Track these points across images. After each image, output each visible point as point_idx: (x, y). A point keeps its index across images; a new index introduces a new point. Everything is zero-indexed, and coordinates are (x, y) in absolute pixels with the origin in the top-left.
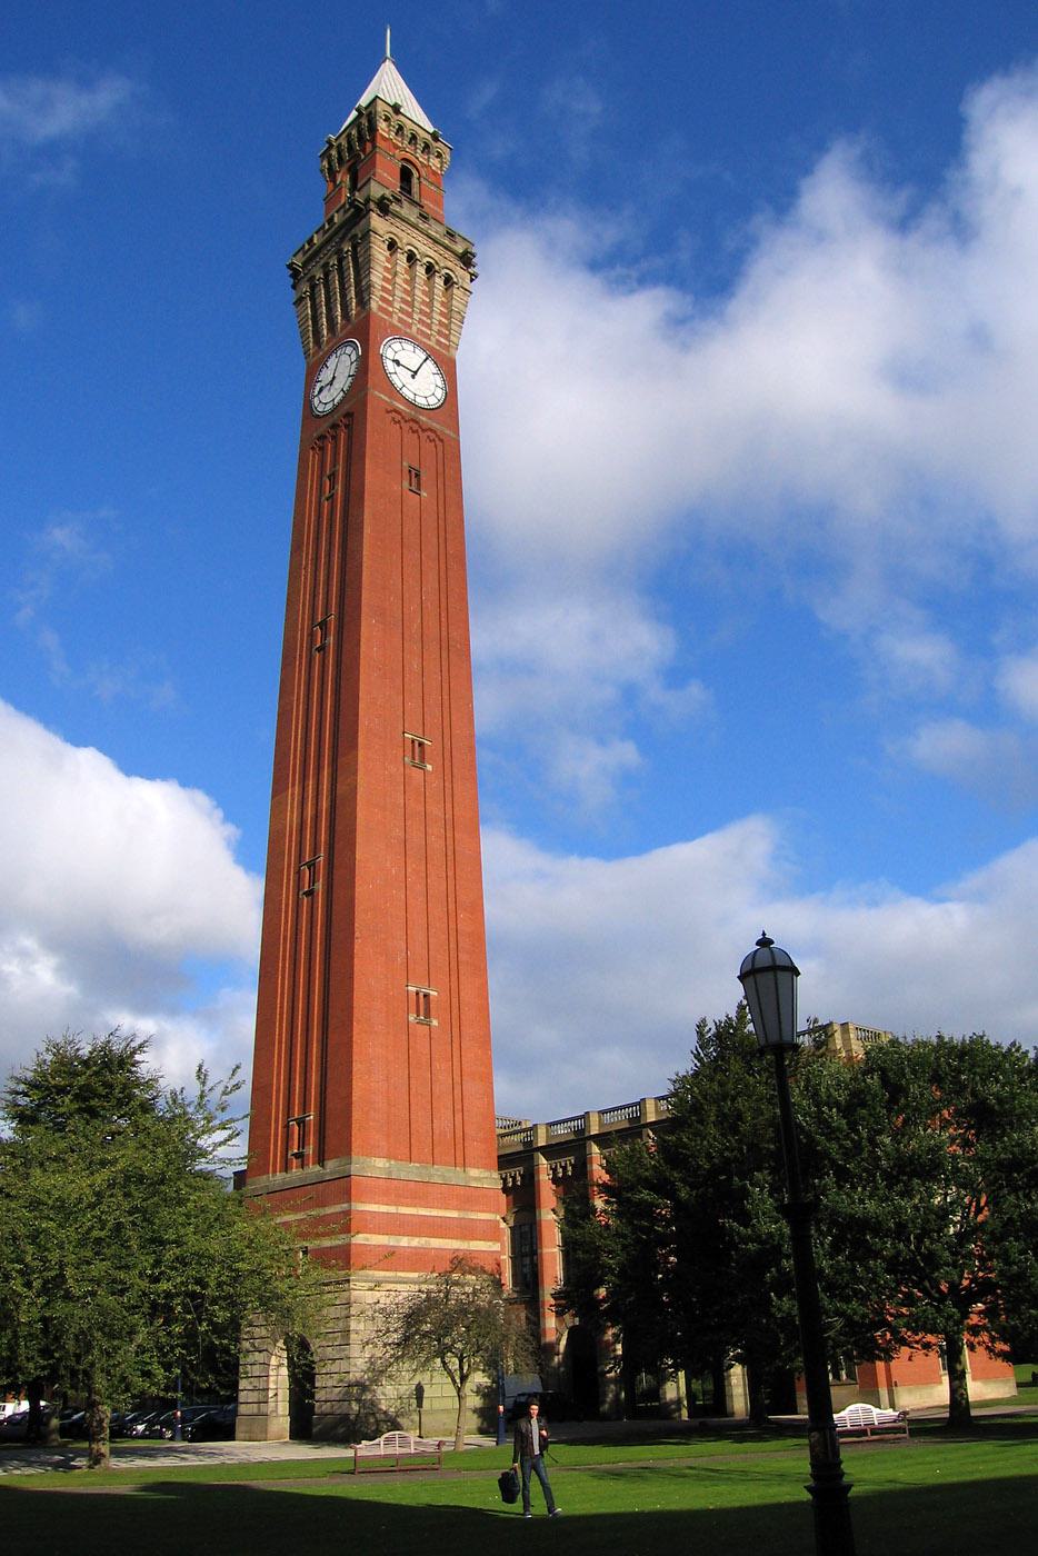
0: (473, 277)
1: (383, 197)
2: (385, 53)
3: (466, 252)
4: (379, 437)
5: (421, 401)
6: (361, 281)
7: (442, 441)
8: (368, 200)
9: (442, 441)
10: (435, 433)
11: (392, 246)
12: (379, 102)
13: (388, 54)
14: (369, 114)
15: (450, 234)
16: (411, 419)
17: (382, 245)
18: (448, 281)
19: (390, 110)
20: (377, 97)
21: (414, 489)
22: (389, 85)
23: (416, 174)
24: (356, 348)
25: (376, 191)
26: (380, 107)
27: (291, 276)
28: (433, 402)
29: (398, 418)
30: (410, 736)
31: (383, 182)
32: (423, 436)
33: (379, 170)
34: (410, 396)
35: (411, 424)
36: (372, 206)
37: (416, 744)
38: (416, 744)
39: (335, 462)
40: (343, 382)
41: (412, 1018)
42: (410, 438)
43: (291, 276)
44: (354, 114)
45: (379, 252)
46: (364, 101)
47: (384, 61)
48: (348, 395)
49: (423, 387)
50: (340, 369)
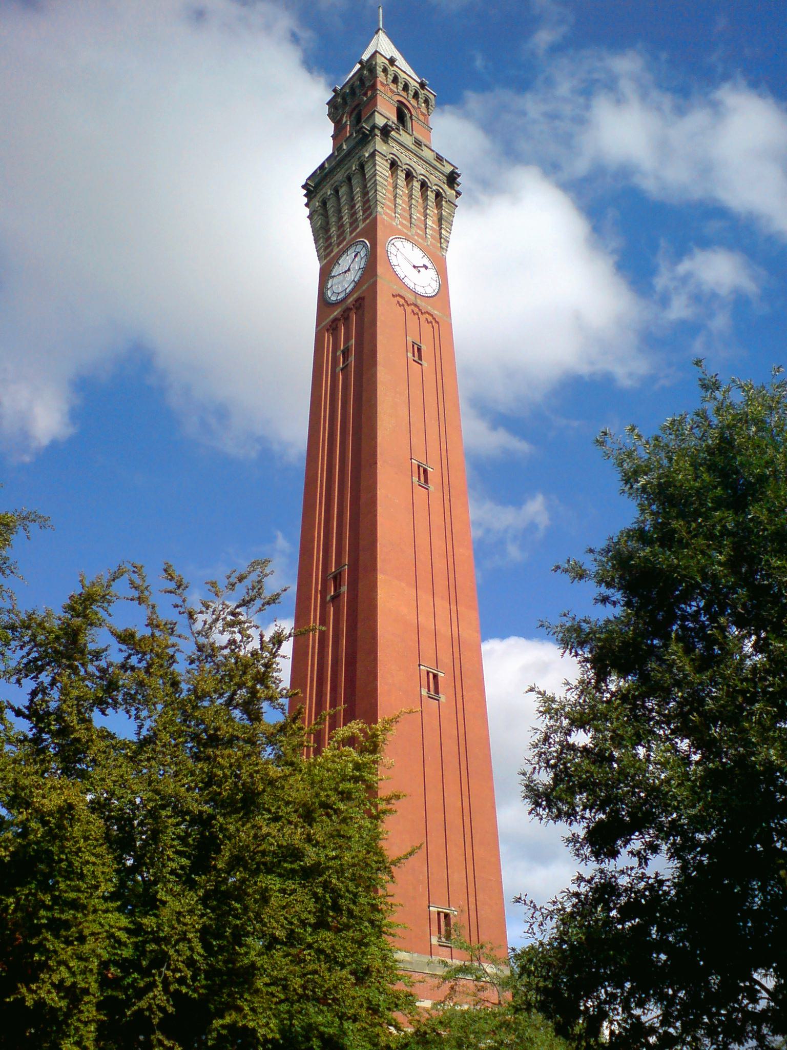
0: (458, 194)
1: (386, 125)
2: (379, 25)
3: (453, 173)
4: (386, 312)
5: (420, 290)
6: (367, 193)
7: (437, 322)
8: (374, 127)
9: (437, 322)
10: (431, 313)
11: (394, 165)
12: (378, 55)
13: (381, 26)
14: (369, 67)
15: (439, 158)
16: (411, 303)
17: (385, 163)
18: (438, 195)
19: (387, 62)
20: (376, 52)
21: (416, 359)
22: (383, 45)
23: (408, 115)
24: (365, 245)
25: (380, 121)
26: (380, 60)
27: (305, 195)
28: (430, 291)
29: (402, 301)
30: (436, 909)
31: (384, 114)
32: (423, 318)
33: (380, 108)
34: (412, 286)
35: (413, 307)
36: (378, 132)
37: (442, 915)
38: (442, 915)
39: (347, 339)
40: (353, 276)
41: (424, 692)
42: (412, 320)
43: (305, 195)
44: (358, 66)
45: (382, 167)
46: (365, 57)
47: (377, 32)
48: (358, 284)
49: (424, 282)
50: (350, 267)
